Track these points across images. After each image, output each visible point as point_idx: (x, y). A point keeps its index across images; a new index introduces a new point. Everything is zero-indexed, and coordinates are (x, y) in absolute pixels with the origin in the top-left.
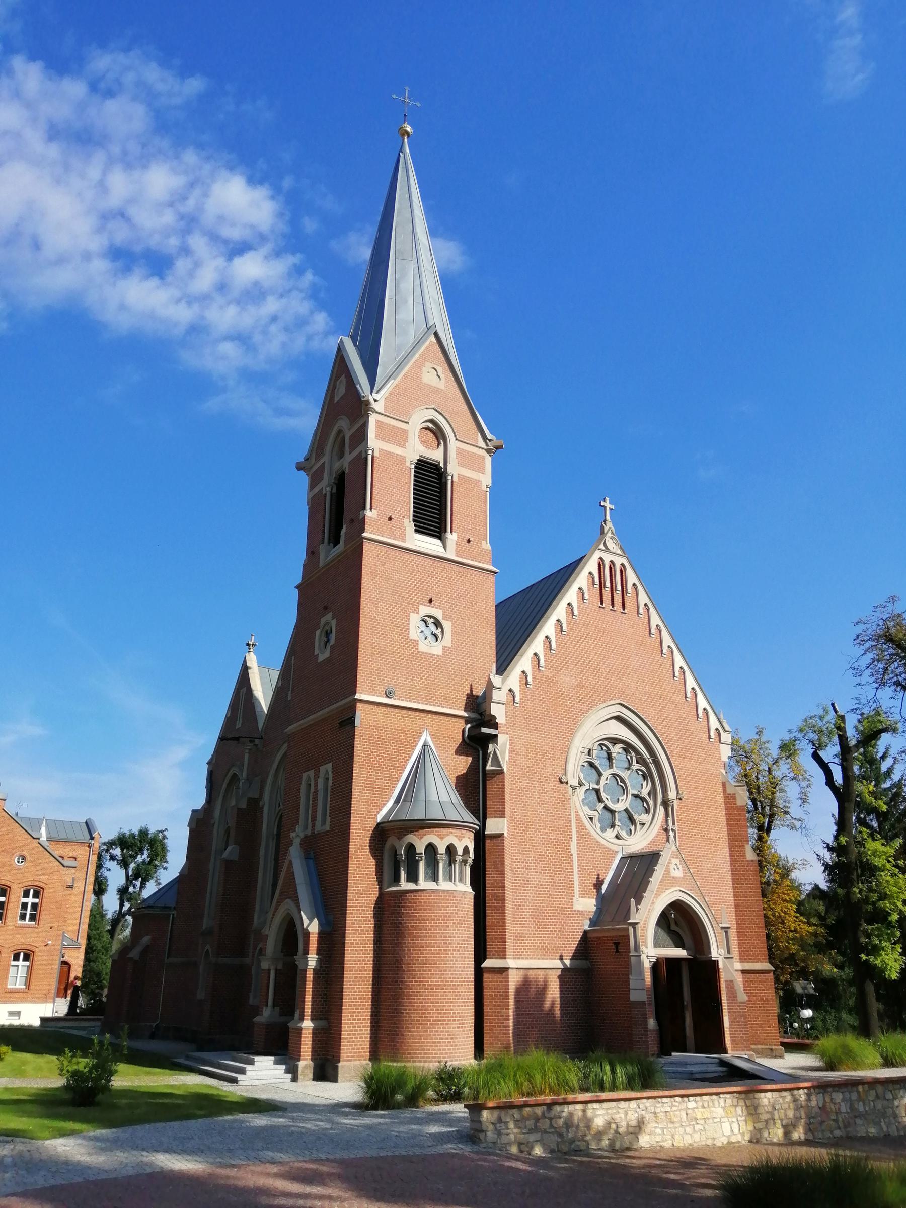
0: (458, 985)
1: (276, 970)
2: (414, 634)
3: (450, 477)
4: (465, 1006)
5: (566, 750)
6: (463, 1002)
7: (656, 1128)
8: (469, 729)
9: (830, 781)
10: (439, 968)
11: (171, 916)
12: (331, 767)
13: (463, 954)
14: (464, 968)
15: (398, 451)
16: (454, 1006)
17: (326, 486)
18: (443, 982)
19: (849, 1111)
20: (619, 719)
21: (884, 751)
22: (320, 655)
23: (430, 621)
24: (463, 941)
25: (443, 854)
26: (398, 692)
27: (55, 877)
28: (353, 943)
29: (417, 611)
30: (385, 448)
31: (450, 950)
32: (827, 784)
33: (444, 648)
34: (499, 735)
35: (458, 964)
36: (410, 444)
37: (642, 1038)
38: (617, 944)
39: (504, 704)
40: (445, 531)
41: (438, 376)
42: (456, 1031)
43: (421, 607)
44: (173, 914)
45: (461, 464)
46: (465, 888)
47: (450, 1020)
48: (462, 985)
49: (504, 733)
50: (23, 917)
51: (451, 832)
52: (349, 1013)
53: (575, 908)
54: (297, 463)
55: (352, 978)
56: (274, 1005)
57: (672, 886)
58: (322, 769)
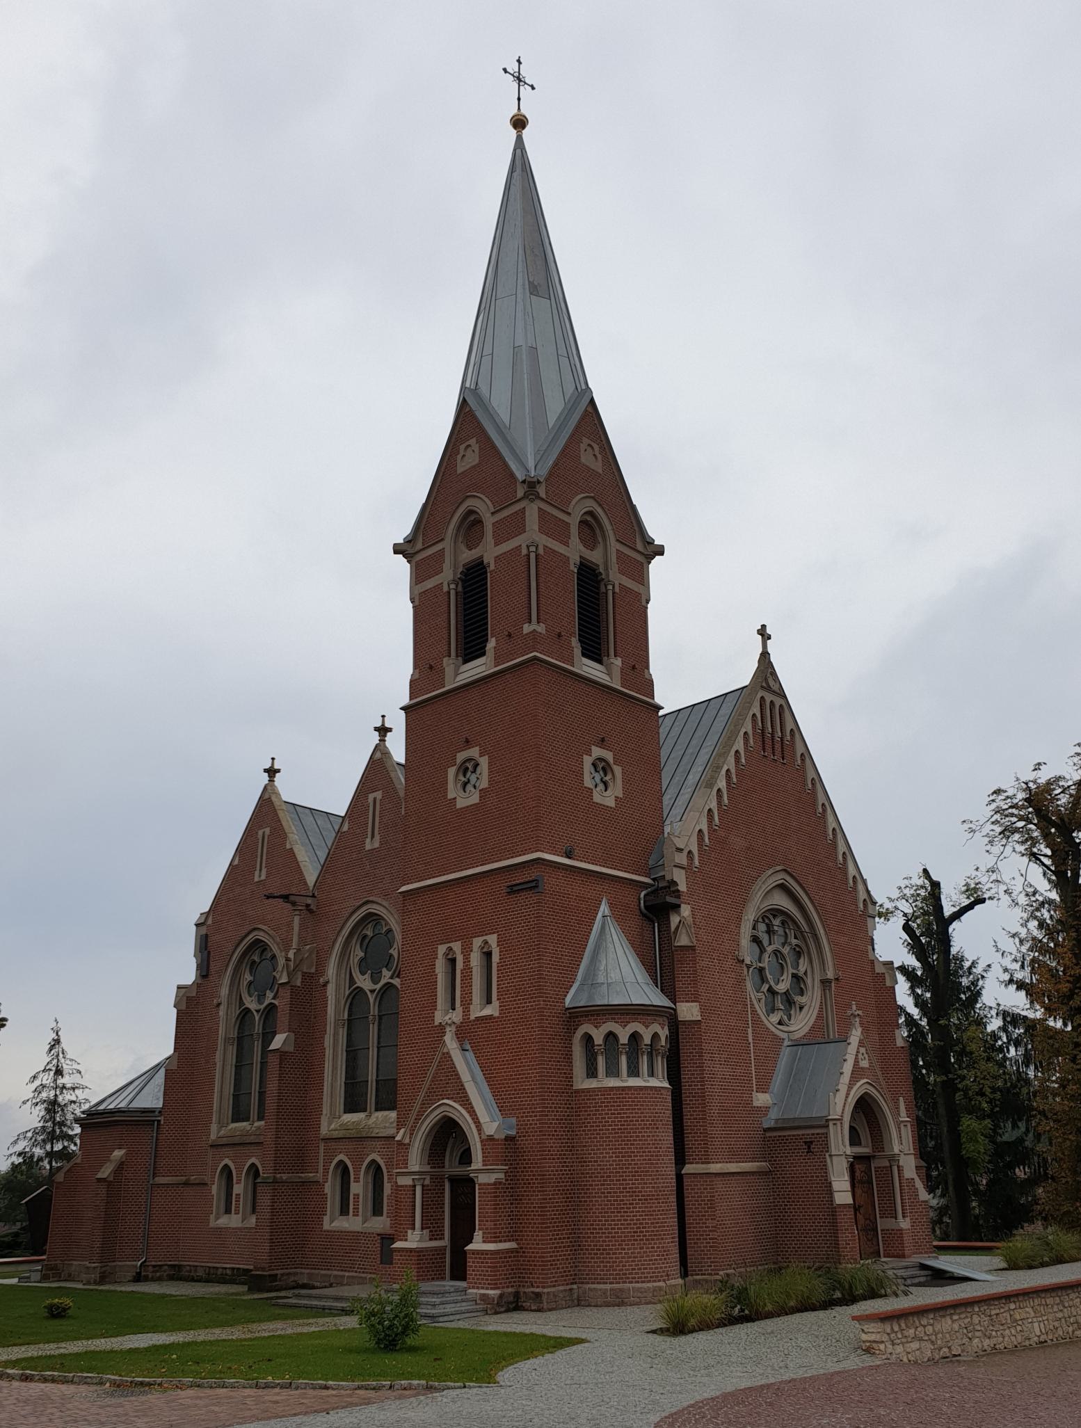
1: (423, 1186)
2: (588, 782)
8: (645, 895)
11: (156, 1123)
12: (496, 940)
15: (561, 549)
17: (447, 576)
20: (783, 887)
22: (458, 800)
23: (601, 765)
25: (601, 1045)
30: (549, 545)
34: (682, 905)
39: (684, 868)
41: (594, 455)
43: (593, 748)
44: (159, 1121)
45: (621, 572)
46: (661, 1082)
51: (655, 1020)
53: (754, 1104)
54: (395, 545)
56: (422, 1229)
57: (861, 1078)
58: (477, 942)
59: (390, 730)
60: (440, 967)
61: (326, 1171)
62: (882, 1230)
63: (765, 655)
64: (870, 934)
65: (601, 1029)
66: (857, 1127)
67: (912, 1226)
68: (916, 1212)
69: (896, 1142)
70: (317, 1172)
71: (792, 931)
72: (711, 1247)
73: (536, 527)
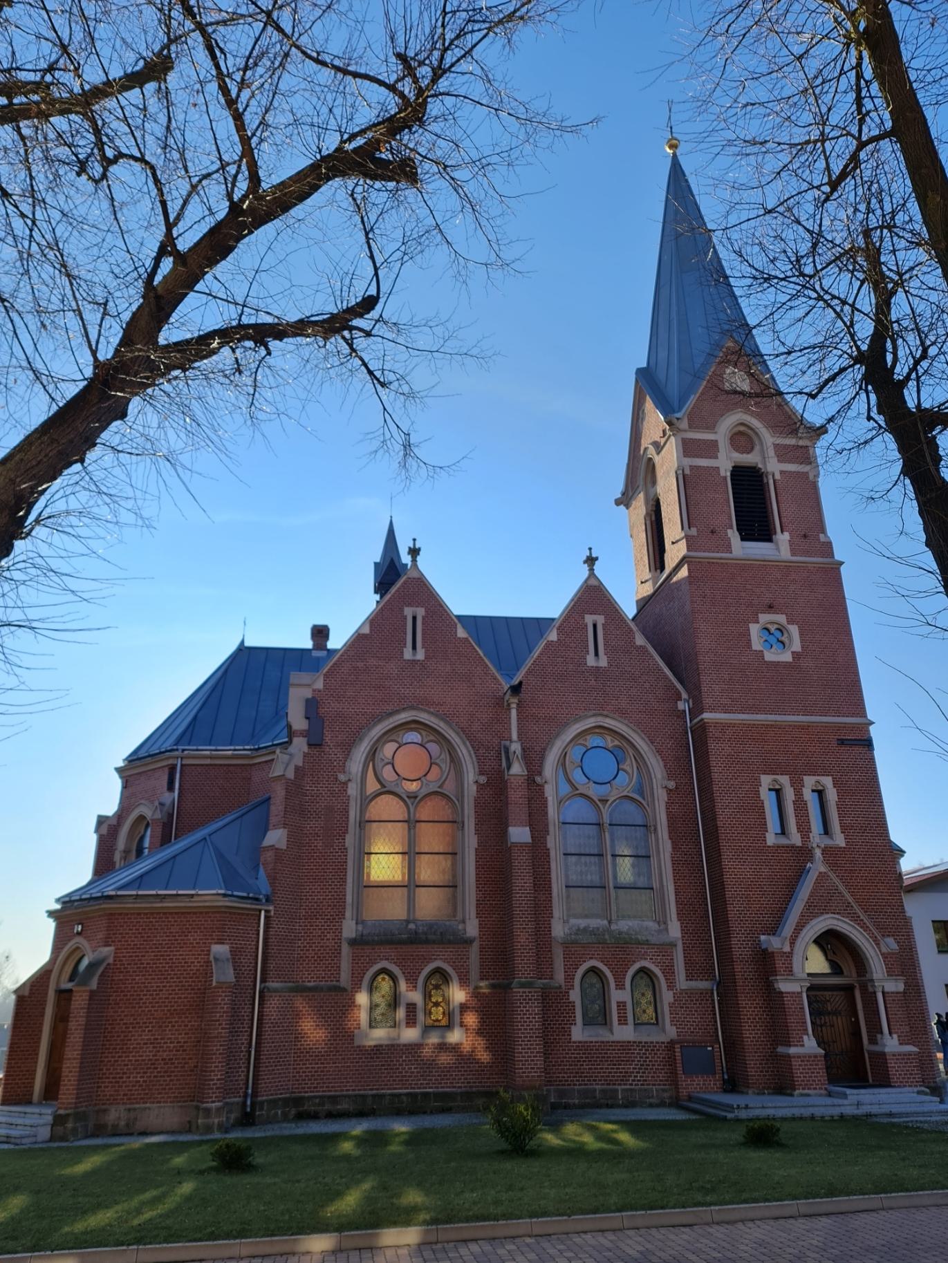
2: (757, 644)
17: (725, 462)
36: (722, 454)
40: (775, 533)
58: (809, 781)
59: (597, 559)
60: (768, 800)
61: (569, 978)
70: (552, 978)
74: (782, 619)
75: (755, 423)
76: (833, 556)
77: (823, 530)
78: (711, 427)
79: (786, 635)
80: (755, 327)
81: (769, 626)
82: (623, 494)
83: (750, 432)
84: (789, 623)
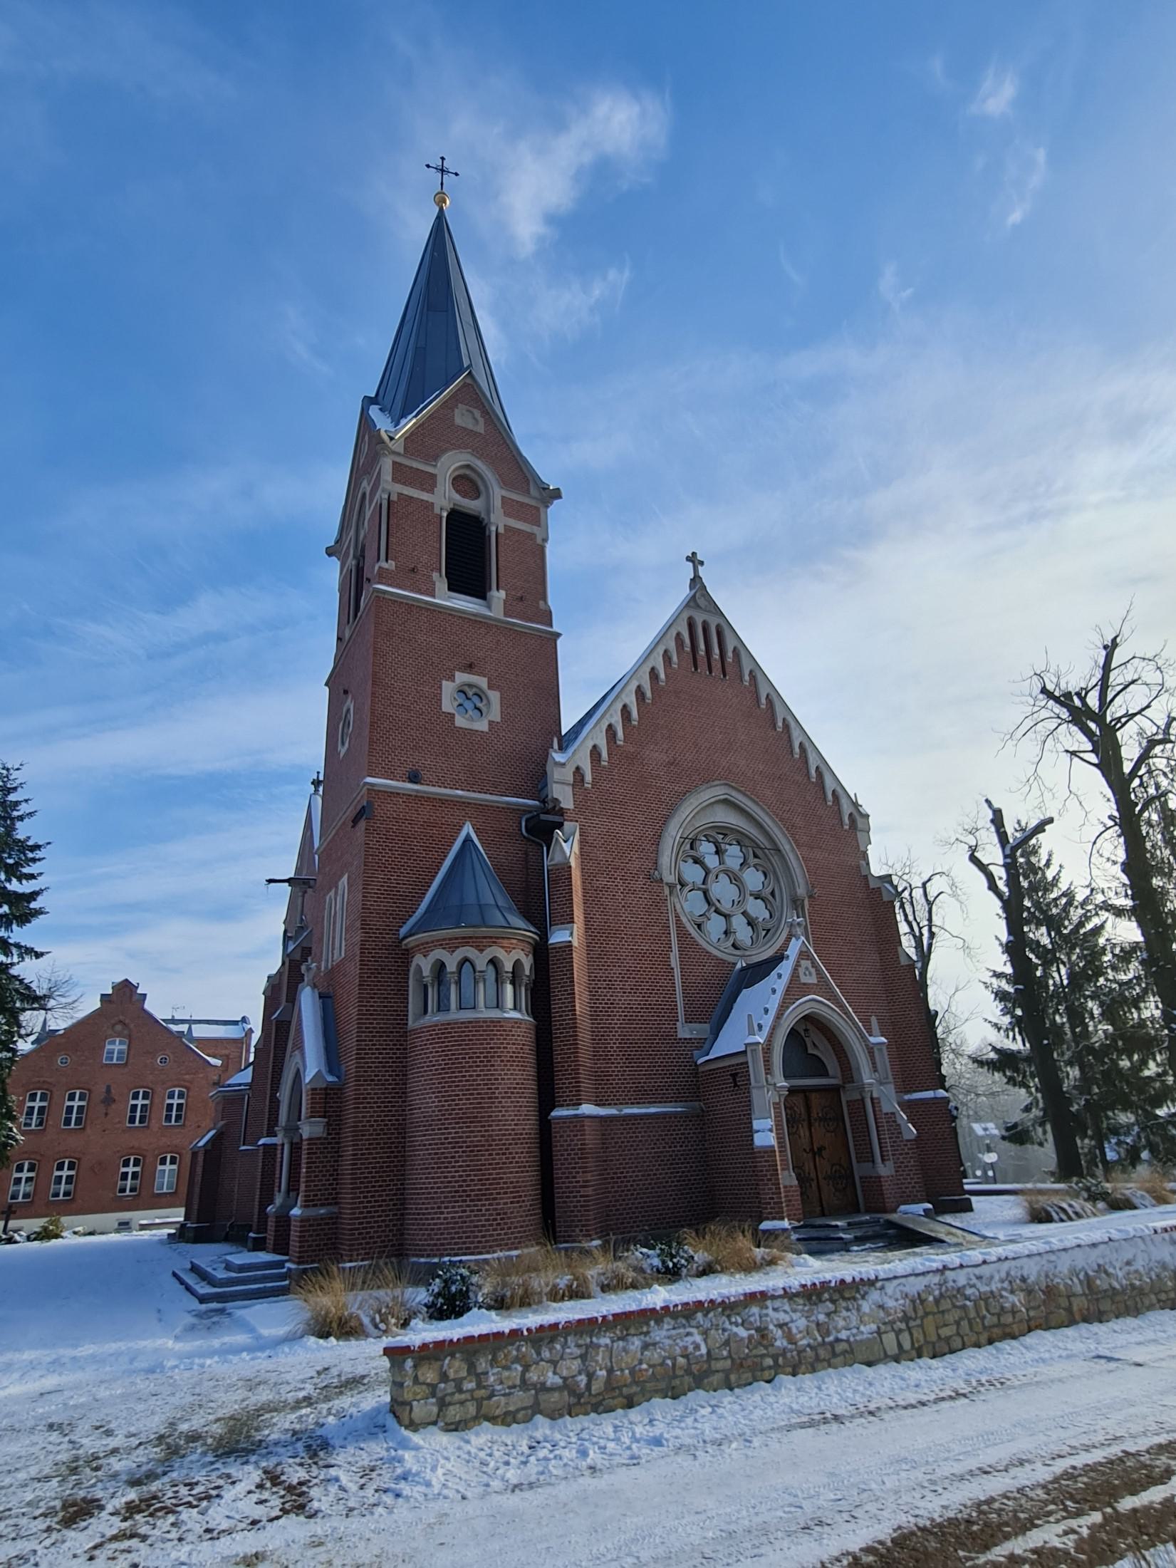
0: (510, 1144)
2: (448, 705)
3: (493, 528)
4: (522, 1172)
5: (657, 839)
6: (519, 1167)
7: (763, 1356)
9: (993, 886)
10: (480, 1122)
13: (518, 1102)
14: (519, 1120)
16: (505, 1173)
17: (444, 498)
18: (487, 1141)
19: (1087, 1292)
20: (726, 802)
21: (1047, 857)
24: (517, 1084)
26: (425, 774)
27: (201, 1075)
28: (366, 1098)
29: (452, 678)
31: (497, 1098)
32: (990, 888)
33: (491, 723)
35: (510, 1116)
36: (439, 489)
37: (773, 1198)
38: (734, 1076)
40: (490, 589)
42: (510, 1208)
43: (457, 674)
45: (507, 514)
47: (499, 1194)
48: (516, 1144)
49: (571, 821)
50: (168, 1118)
52: (361, 1193)
55: (364, 1145)
62: (861, 1178)
63: (696, 581)
64: (862, 849)
65: (429, 958)
66: (823, 1059)
67: (897, 1171)
68: (901, 1154)
69: (867, 1070)
71: (750, 849)
72: (581, 1206)
73: (389, 478)
74: (482, 682)
75: (480, 465)
76: (551, 626)
77: (544, 598)
78: (434, 458)
79: (485, 701)
80: (569, 784)
81: (466, 689)
82: (337, 542)
83: (480, 483)
84: (490, 687)
